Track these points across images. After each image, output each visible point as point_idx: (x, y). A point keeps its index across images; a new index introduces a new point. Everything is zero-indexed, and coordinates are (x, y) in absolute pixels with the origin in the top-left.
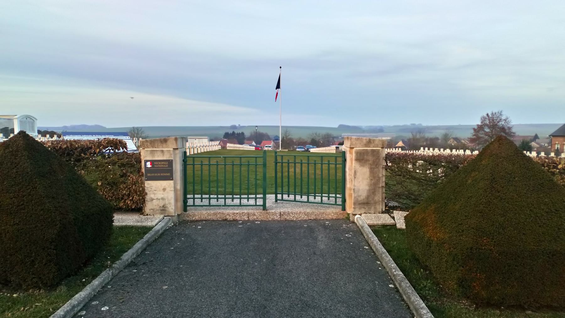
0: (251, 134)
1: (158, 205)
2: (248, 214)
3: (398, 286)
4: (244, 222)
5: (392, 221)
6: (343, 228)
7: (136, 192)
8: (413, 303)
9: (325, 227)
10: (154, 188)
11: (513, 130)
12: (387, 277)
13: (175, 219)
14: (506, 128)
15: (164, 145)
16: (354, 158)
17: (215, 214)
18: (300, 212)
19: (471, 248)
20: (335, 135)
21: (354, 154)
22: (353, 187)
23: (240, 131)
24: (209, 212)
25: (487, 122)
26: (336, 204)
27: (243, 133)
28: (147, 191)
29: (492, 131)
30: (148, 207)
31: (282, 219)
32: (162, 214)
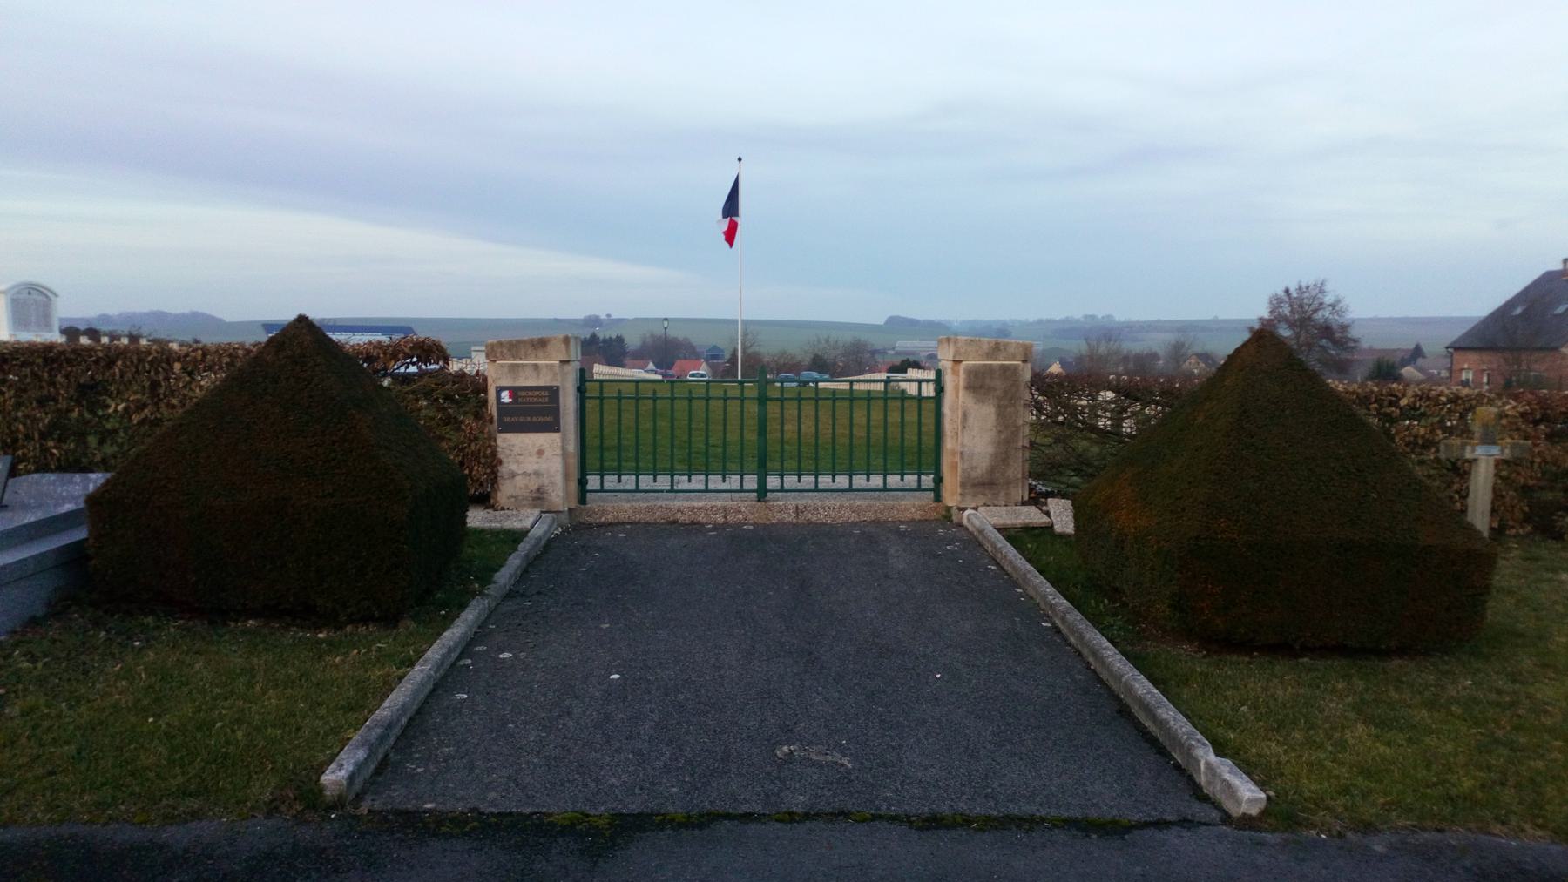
0: (644, 344)
1: (527, 487)
2: (725, 509)
3: (1058, 622)
4: (716, 527)
5: (1045, 519)
6: (939, 537)
7: (477, 459)
8: (1086, 644)
9: (902, 535)
10: (516, 450)
11: (1354, 333)
12: (1034, 611)
13: (564, 518)
14: (1335, 327)
15: (541, 354)
16: (962, 383)
17: (651, 510)
18: (841, 506)
19: (1197, 538)
20: (878, 346)
21: (962, 376)
22: (959, 449)
23: (612, 333)
24: (636, 504)
25: (1286, 310)
26: (919, 489)
27: (620, 339)
28: (501, 456)
29: (1298, 336)
30: (506, 491)
31: (802, 519)
32: (535, 507)
